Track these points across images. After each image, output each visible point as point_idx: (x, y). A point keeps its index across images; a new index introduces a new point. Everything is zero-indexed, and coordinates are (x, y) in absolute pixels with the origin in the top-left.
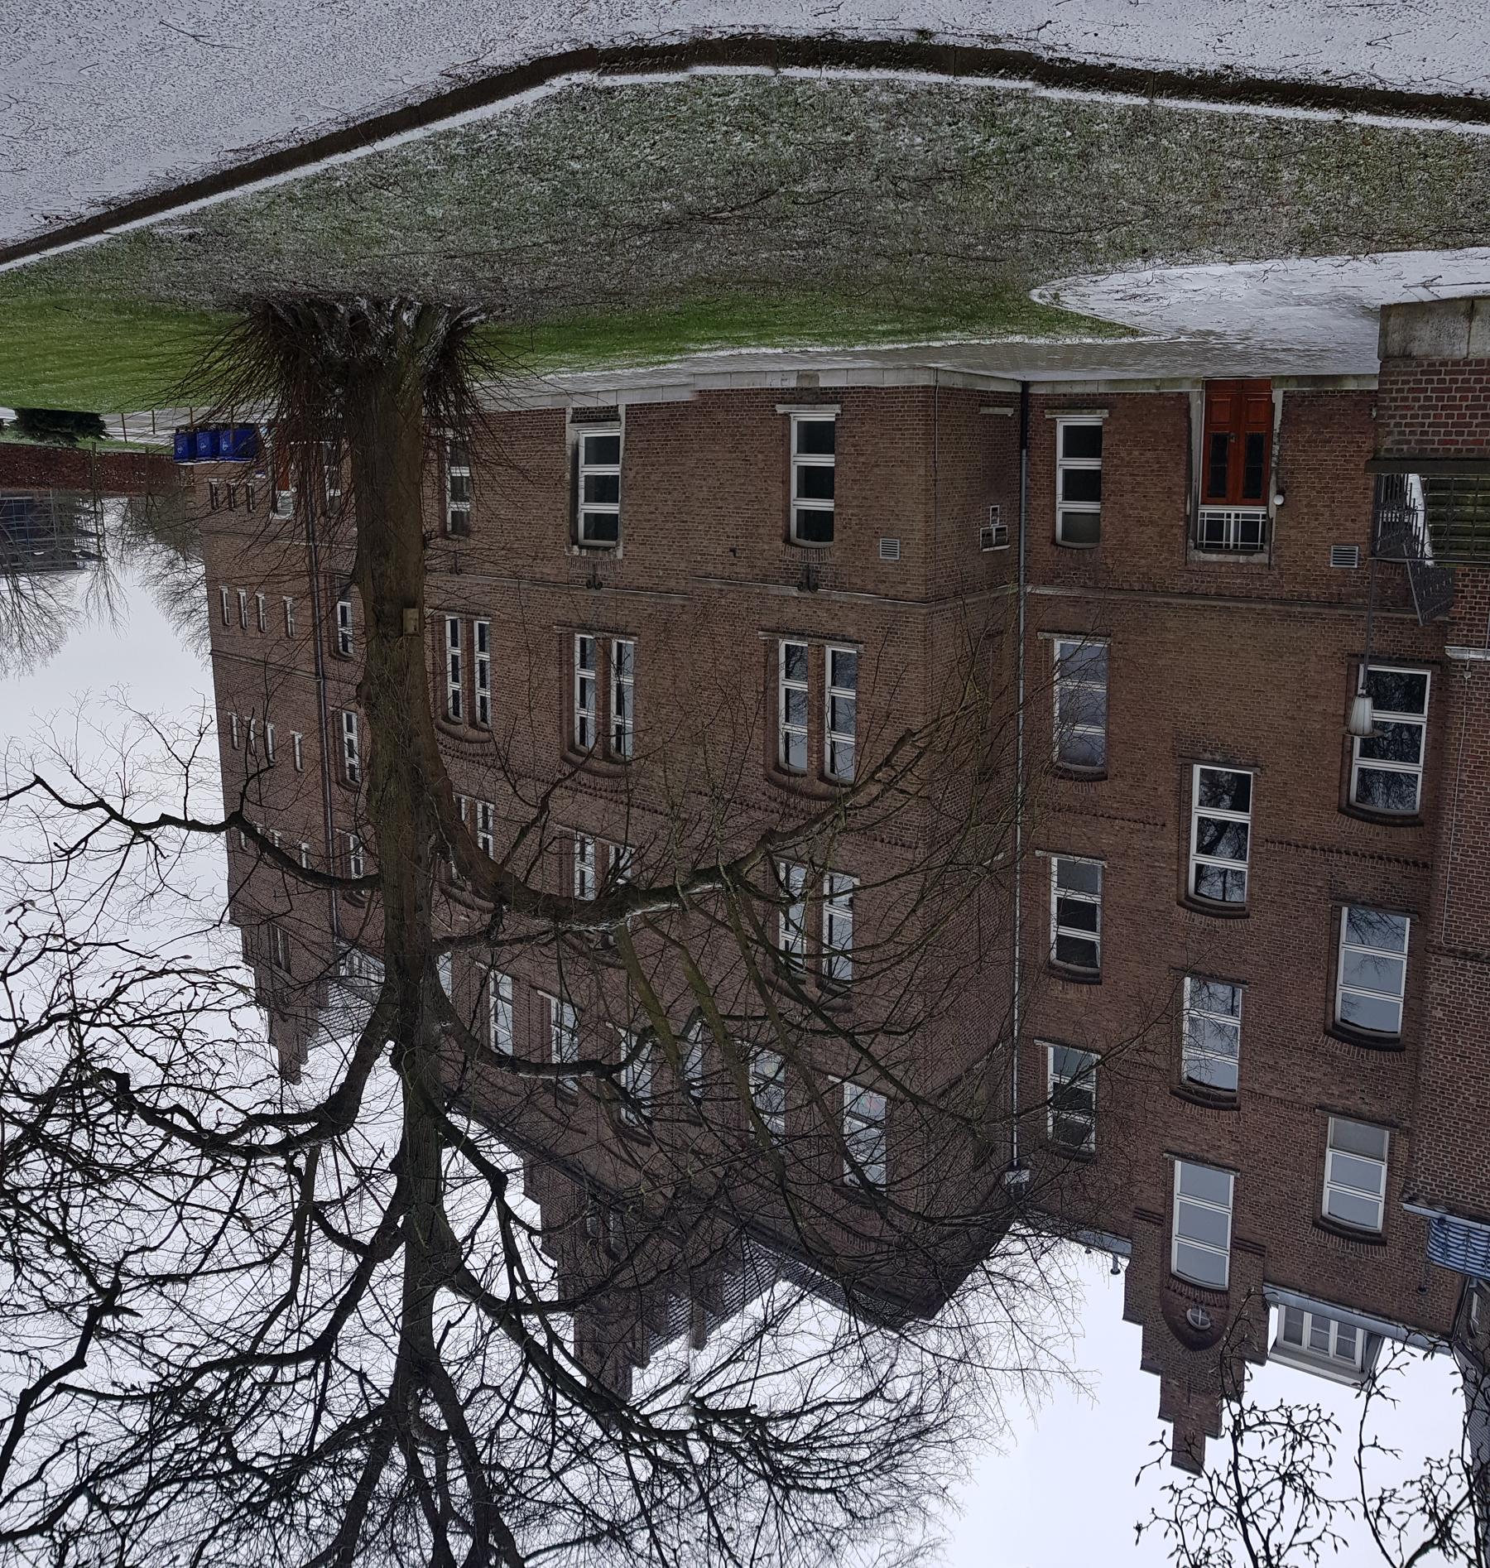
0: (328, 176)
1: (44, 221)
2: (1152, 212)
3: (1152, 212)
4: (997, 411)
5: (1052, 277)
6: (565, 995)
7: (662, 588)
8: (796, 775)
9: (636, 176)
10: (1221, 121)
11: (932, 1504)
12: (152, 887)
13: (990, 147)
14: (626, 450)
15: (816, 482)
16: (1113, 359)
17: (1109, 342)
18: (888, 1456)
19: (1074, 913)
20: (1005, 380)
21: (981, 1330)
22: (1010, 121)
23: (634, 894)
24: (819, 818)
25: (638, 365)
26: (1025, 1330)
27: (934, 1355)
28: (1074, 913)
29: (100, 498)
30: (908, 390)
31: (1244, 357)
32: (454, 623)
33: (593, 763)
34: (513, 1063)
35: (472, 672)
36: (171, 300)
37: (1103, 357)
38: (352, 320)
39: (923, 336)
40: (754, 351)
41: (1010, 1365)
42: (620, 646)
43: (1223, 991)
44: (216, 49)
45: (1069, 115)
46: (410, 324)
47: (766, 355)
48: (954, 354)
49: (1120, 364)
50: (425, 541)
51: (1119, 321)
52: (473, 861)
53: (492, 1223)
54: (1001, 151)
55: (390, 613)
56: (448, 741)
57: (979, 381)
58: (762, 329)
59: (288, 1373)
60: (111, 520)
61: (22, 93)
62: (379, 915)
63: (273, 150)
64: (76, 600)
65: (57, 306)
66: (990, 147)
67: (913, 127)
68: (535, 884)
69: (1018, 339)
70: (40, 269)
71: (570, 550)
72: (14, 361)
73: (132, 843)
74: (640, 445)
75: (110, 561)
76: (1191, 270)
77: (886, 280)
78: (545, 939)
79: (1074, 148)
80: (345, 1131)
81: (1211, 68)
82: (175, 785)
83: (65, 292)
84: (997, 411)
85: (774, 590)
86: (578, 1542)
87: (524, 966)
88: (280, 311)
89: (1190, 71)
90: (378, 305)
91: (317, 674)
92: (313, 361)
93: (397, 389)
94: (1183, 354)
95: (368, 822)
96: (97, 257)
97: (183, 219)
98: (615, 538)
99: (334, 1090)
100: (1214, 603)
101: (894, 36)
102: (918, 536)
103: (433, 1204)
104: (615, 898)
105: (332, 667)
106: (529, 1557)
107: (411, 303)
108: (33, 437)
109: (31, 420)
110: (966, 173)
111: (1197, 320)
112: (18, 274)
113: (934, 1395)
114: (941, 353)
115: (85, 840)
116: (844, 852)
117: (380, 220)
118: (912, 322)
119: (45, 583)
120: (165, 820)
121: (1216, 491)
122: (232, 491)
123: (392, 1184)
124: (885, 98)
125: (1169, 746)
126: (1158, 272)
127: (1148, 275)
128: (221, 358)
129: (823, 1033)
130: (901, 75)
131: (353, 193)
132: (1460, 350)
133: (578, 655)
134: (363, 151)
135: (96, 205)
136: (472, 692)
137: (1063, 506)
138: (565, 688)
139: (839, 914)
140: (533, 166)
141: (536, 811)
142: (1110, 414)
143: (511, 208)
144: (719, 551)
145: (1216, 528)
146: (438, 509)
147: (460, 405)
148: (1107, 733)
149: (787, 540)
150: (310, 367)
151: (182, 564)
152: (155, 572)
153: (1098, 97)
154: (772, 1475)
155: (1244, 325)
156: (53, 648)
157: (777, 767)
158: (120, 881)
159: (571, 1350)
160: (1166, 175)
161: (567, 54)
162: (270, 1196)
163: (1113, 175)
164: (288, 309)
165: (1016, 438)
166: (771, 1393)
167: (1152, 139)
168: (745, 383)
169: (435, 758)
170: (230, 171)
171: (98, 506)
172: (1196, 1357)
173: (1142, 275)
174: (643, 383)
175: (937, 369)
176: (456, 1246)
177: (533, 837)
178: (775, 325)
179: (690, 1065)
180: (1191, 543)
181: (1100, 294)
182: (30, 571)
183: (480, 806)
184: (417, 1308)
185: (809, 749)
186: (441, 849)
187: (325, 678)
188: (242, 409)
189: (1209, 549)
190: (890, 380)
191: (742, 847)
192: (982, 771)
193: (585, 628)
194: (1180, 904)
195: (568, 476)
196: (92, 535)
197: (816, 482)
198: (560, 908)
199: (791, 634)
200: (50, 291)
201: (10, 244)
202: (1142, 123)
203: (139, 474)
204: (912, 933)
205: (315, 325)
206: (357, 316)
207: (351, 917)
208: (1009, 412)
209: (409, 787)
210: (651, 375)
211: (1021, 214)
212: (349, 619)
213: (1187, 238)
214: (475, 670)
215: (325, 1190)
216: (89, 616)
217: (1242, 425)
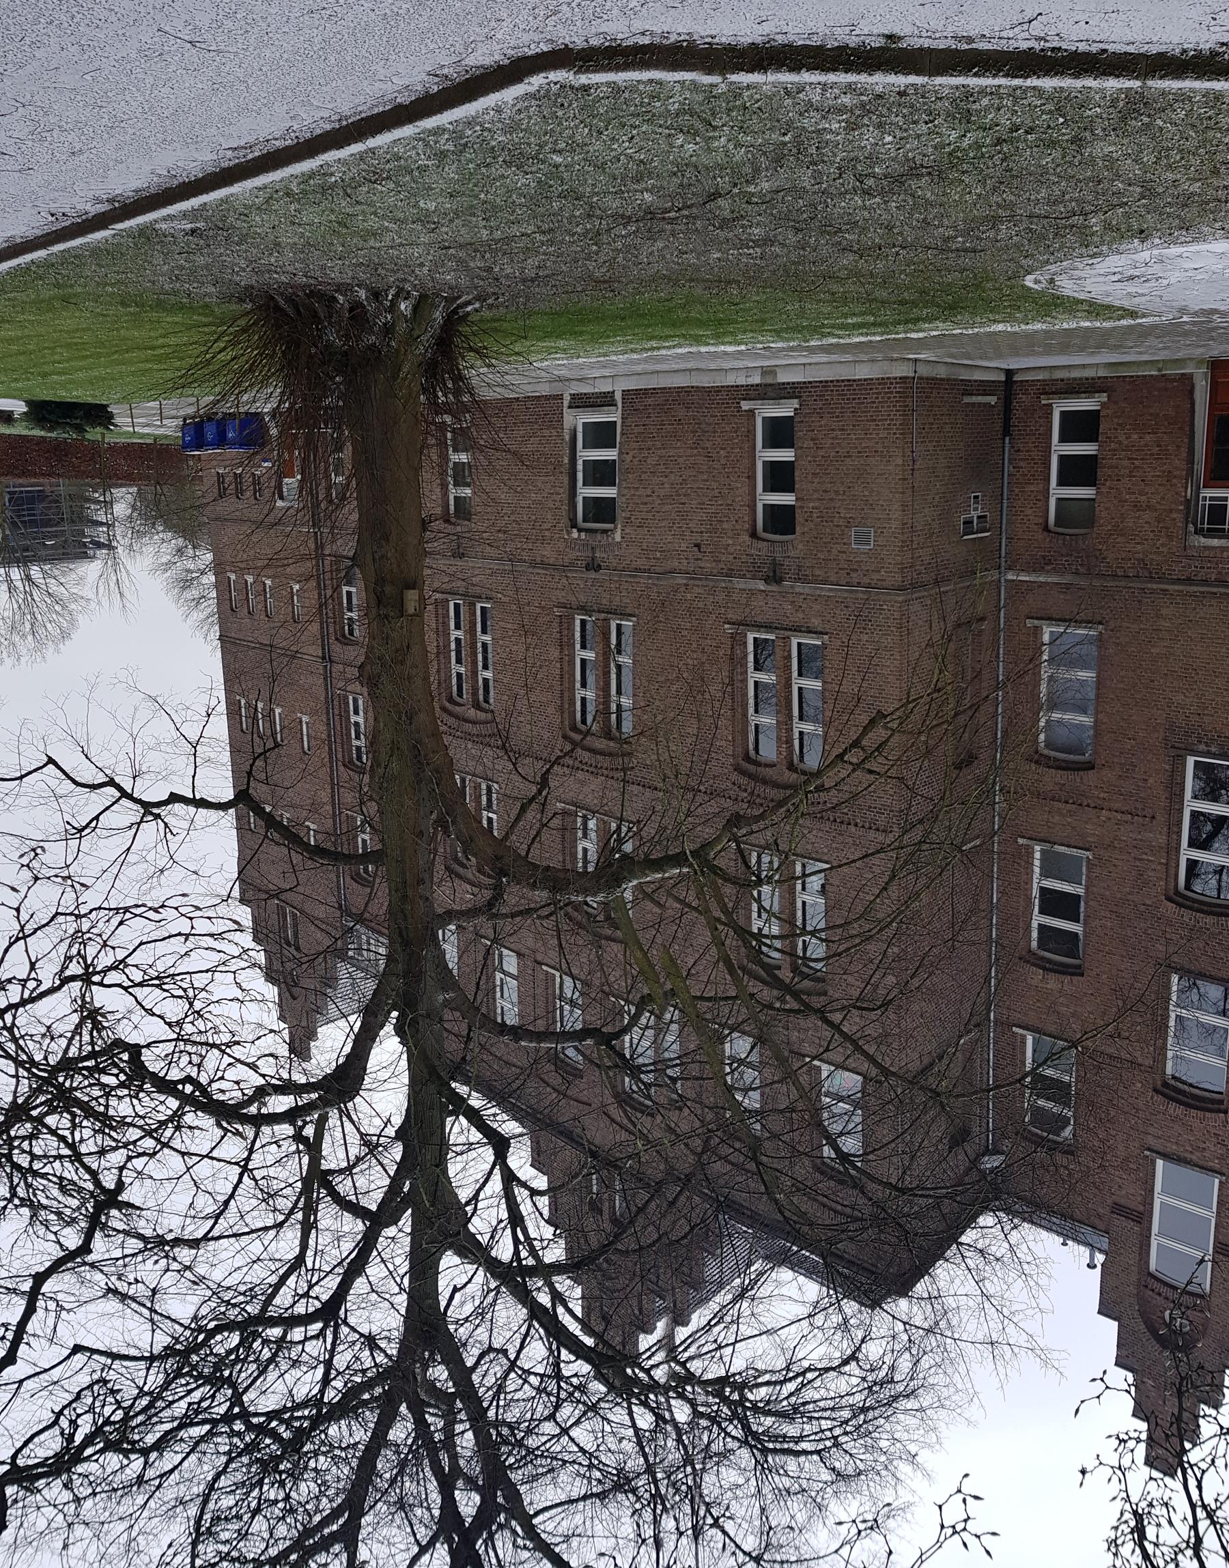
0: (323, 172)
1: (50, 218)
2: (1148, 191)
3: (1148, 191)
4: (980, 399)
5: (1047, 262)
6: (564, 966)
7: (658, 569)
8: (766, 765)
9: (617, 169)
10: (1217, 98)
11: (904, 1468)
12: (162, 863)
13: (966, 143)
14: (622, 434)
15: (780, 477)
16: (1112, 342)
17: (1106, 324)
19: (1055, 903)
20: (990, 368)
21: (951, 1302)
22: (985, 117)
24: (781, 804)
25: (632, 351)
26: (995, 1303)
27: (905, 1323)
29: (110, 487)
30: (882, 381)
32: (457, 606)
33: (592, 741)
34: (516, 1033)
35: (475, 654)
36: (175, 293)
37: (1101, 340)
38: (351, 310)
39: (901, 328)
40: (712, 349)
41: (980, 1337)
42: (619, 627)
44: (212, 54)
45: (1061, 100)
46: (408, 313)
47: (725, 353)
48: (934, 345)
49: (1121, 346)
50: (424, 525)
51: (1117, 303)
52: (474, 836)
53: (496, 1184)
54: (978, 146)
55: (389, 597)
56: (451, 721)
57: (963, 370)
58: (721, 328)
59: (297, 1334)
60: (121, 509)
61: (28, 96)
63: (270, 148)
64: (86, 588)
65: (65, 300)
66: (966, 143)
67: (880, 126)
69: (1000, 327)
70: (47, 264)
71: (569, 533)
72: (24, 353)
73: (141, 821)
74: (636, 430)
75: (120, 550)
76: (1191, 249)
77: (856, 274)
78: (546, 911)
79: (1067, 134)
80: (352, 1099)
81: (1205, 47)
82: (183, 765)
83: (72, 286)
84: (980, 399)
85: (739, 583)
86: (584, 1498)
87: (528, 940)
88: (282, 302)
89: (1184, 51)
90: (376, 295)
91: (324, 658)
92: (313, 350)
93: (395, 377)
94: (1186, 334)
95: (371, 799)
96: (97, 257)
97: (184, 215)
98: (612, 520)
99: (341, 1061)
100: (1215, 590)
101: (853, 42)
102: (894, 525)
103: (437, 1166)
104: (613, 870)
106: (537, 1514)
107: (408, 292)
108: (43, 428)
109: (41, 411)
110: (944, 168)
111: (1199, 299)
112: (25, 270)
113: (905, 1364)
114: (921, 344)
115: (97, 818)
116: (815, 835)
117: (375, 213)
118: (887, 314)
119: (56, 572)
120: (174, 798)
123: (397, 1152)
124: (846, 100)
125: (1162, 735)
126: (1155, 252)
127: (1146, 255)
128: (224, 349)
129: (798, 1012)
130: (863, 78)
131: (348, 188)
133: (578, 635)
135: (101, 202)
136: (475, 673)
137: (1057, 492)
138: (566, 669)
140: (517, 159)
141: (534, 789)
142: (1109, 396)
143: (498, 200)
144: (684, 546)
147: (457, 392)
148: (1096, 722)
149: (754, 535)
150: (311, 356)
151: (190, 552)
152: (164, 560)
153: (1090, 82)
154: (751, 1439)
156: (65, 635)
157: (747, 758)
158: (131, 858)
159: (578, 1311)
160: (1162, 153)
161: (544, 53)
162: (279, 1161)
163: (1108, 158)
164: (289, 300)
165: (998, 426)
166: (749, 1354)
167: (1146, 120)
168: (705, 381)
169: (436, 735)
170: (229, 168)
171: (108, 494)
173: (1142, 255)
174: (639, 368)
175: (916, 360)
176: (461, 1207)
177: (532, 814)
178: (737, 323)
179: (666, 1045)
180: (1191, 528)
181: (1101, 276)
183: (484, 786)
185: (779, 738)
186: (441, 823)
187: (331, 661)
188: (245, 398)
189: (1211, 533)
190: (863, 372)
191: (708, 832)
192: (963, 754)
193: (583, 609)
194: (1169, 899)
195: (566, 460)
196: (102, 524)
197: (780, 477)
198: (558, 880)
199: (758, 626)
200: (58, 286)
201: (19, 240)
202: (1135, 105)
203: (148, 465)
204: (884, 909)
205: (315, 315)
206: (356, 306)
207: (357, 896)
208: (993, 400)
209: (411, 762)
210: (646, 360)
211: (999, 205)
212: (355, 601)
214: (476, 649)
215: (333, 1157)
216: (99, 603)
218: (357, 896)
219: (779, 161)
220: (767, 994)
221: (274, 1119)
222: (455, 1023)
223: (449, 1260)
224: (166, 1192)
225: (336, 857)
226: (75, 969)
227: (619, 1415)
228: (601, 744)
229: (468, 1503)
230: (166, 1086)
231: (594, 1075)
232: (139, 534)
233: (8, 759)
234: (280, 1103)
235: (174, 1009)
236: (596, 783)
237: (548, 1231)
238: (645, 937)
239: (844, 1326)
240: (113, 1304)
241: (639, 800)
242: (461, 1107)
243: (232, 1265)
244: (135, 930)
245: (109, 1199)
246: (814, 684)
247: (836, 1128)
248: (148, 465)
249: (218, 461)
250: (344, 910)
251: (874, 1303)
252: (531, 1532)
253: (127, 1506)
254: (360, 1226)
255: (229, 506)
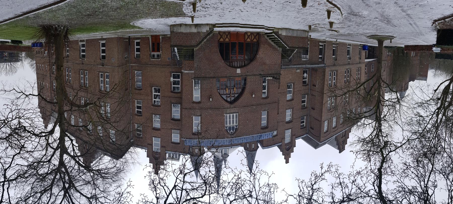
0: (52, 9)
9: (84, 8)
11: (122, 180)
15: (104, 51)
18: (116, 174)
19: (138, 107)
20: (127, 36)
23: (88, 104)
28: (138, 107)
31: (156, 32)
33: (83, 88)
34: (74, 126)
37: (136, 32)
43: (158, 116)
48: (120, 33)
50: (64, 58)
52: (69, 100)
53: (71, 145)
58: (96, 30)
59: (45, 164)
60: (23, 55)
62: (57, 107)
68: (76, 103)
70: (14, 21)
82: (31, 90)
85: (99, 66)
87: (75, 114)
90: (59, 26)
96: (19, 21)
104: (86, 105)
105: (52, 75)
109: (13, 42)
112: (11, 22)
113: (122, 167)
116: (109, 100)
118: (115, 28)
120: (30, 94)
121: (153, 51)
122: (39, 51)
123: (58, 141)
131: (55, 11)
132: (180, 31)
134: (57, 5)
139: (108, 109)
140: (74, 7)
145: (154, 56)
146: (65, 54)
154: (102, 177)
155: (155, 28)
156: (16, 72)
162: (43, 141)
169: (65, 87)
172: (157, 161)
177: (76, 97)
182: (13, 62)
184: (61, 156)
186: (65, 99)
190: (113, 36)
191: (96, 100)
192: (126, 89)
193: (82, 70)
197: (104, 51)
198: (79, 106)
203: (28, 49)
204: (117, 109)
206: (56, 28)
207: (54, 108)
209: (61, 91)
213: (147, 15)
214: (69, 75)
215: (50, 141)
217: (156, 41)
218: (54, 108)
219: (103, 7)
220: (103, 121)
221: (43, 136)
222: (66, 125)
223: (65, 155)
224: (29, 146)
225: (51, 103)
226: (18, 116)
227: (89, 174)
228: (84, 88)
229: (67, 186)
230: (29, 132)
231: (84, 131)
232: (26, 59)
233: (7, 89)
234: (44, 134)
235: (30, 122)
236: (83, 93)
237: (78, 151)
238: (90, 113)
239: (114, 163)
240: (21, 159)
241: (89, 95)
242: (67, 136)
243: (37, 155)
244: (26, 112)
245: (23, 147)
246: (108, 80)
247: (112, 138)
248: (28, 49)
249: (36, 49)
250: (52, 110)
251: (117, 159)
252: (76, 189)
253: (23, 184)
254: (53, 150)
255: (38, 55)
